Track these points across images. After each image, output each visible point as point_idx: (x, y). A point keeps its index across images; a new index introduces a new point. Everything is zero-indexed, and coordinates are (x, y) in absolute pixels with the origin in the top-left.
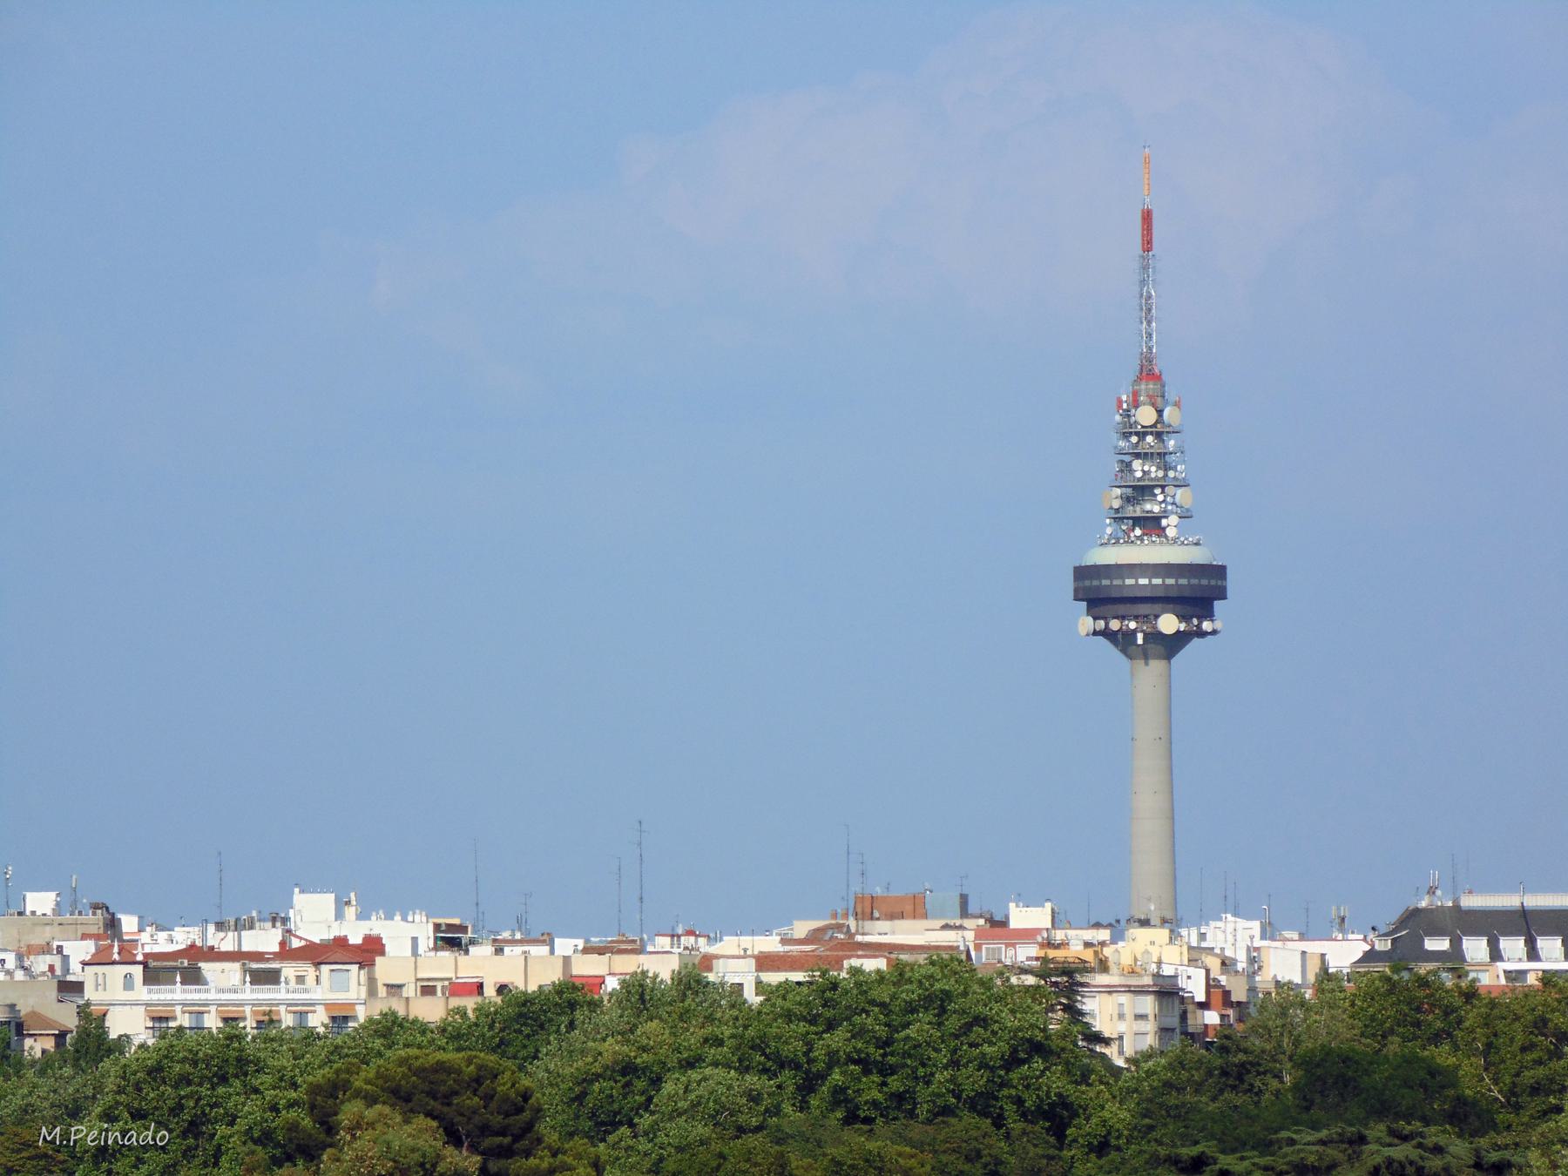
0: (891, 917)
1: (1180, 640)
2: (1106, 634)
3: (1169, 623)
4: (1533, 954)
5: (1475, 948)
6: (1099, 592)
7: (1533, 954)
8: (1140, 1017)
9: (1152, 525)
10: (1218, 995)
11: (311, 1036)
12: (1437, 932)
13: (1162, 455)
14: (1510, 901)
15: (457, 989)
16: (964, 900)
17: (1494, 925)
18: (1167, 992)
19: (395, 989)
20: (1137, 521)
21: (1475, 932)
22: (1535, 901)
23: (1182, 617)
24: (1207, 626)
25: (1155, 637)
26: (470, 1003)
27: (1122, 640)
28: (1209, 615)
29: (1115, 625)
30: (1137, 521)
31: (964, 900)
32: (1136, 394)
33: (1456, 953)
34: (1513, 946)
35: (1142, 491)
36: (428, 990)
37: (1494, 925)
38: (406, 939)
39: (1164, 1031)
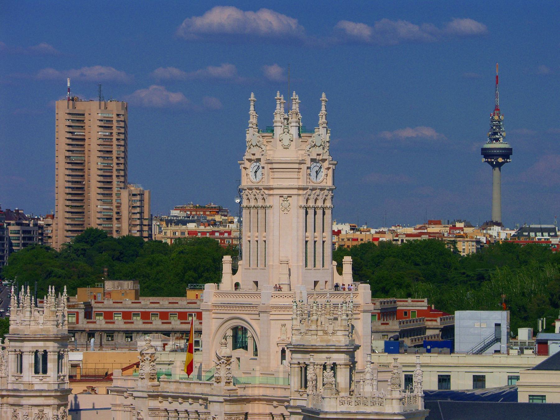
0: (435, 224)
1: (502, 163)
2: (488, 162)
3: (500, 160)
4: (542, 235)
5: (532, 234)
6: (486, 153)
7: (542, 235)
8: (473, 246)
9: (497, 140)
10: (488, 242)
11: (273, 123)
12: (526, 232)
13: (499, 126)
14: (539, 226)
15: (354, 240)
16: (448, 221)
17: (536, 230)
18: (478, 242)
19: (343, 240)
20: (494, 139)
21: (532, 231)
22: (543, 226)
23: (503, 159)
24: (508, 160)
25: (497, 162)
26: (355, 243)
27: (491, 163)
28: (508, 158)
29: (489, 160)
30: (494, 139)
31: (448, 221)
32: (494, 113)
33: (529, 235)
34: (539, 234)
35: (496, 133)
36: (349, 240)
37: (536, 230)
38: (345, 228)
39: (477, 249)
